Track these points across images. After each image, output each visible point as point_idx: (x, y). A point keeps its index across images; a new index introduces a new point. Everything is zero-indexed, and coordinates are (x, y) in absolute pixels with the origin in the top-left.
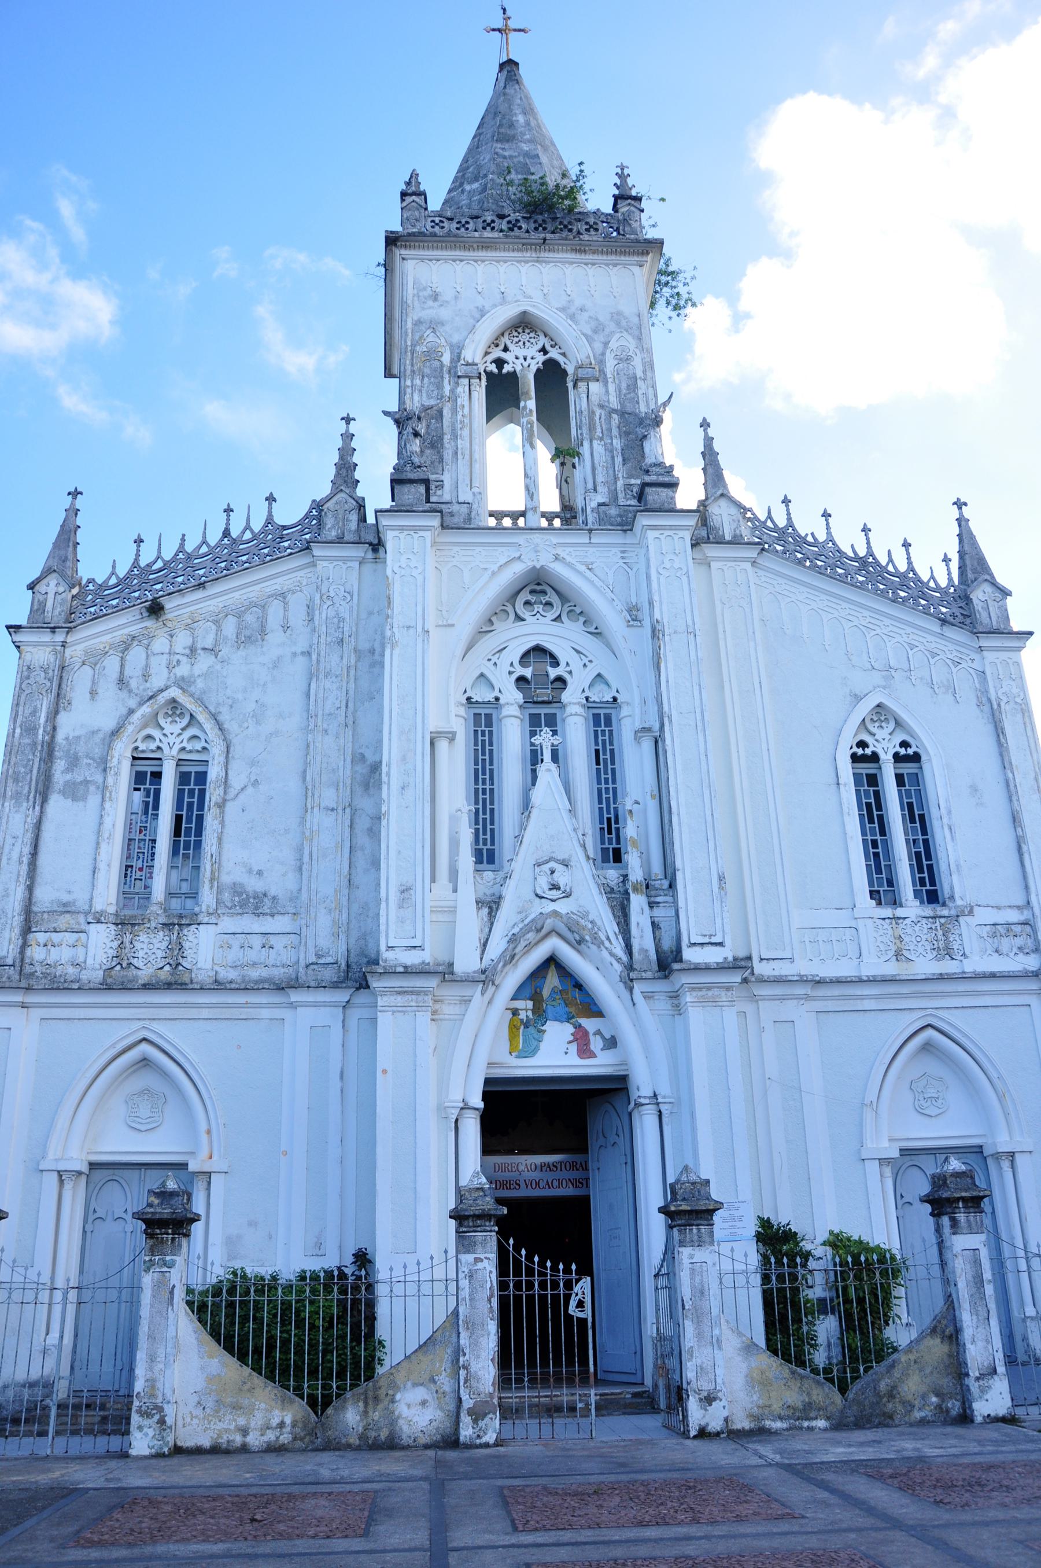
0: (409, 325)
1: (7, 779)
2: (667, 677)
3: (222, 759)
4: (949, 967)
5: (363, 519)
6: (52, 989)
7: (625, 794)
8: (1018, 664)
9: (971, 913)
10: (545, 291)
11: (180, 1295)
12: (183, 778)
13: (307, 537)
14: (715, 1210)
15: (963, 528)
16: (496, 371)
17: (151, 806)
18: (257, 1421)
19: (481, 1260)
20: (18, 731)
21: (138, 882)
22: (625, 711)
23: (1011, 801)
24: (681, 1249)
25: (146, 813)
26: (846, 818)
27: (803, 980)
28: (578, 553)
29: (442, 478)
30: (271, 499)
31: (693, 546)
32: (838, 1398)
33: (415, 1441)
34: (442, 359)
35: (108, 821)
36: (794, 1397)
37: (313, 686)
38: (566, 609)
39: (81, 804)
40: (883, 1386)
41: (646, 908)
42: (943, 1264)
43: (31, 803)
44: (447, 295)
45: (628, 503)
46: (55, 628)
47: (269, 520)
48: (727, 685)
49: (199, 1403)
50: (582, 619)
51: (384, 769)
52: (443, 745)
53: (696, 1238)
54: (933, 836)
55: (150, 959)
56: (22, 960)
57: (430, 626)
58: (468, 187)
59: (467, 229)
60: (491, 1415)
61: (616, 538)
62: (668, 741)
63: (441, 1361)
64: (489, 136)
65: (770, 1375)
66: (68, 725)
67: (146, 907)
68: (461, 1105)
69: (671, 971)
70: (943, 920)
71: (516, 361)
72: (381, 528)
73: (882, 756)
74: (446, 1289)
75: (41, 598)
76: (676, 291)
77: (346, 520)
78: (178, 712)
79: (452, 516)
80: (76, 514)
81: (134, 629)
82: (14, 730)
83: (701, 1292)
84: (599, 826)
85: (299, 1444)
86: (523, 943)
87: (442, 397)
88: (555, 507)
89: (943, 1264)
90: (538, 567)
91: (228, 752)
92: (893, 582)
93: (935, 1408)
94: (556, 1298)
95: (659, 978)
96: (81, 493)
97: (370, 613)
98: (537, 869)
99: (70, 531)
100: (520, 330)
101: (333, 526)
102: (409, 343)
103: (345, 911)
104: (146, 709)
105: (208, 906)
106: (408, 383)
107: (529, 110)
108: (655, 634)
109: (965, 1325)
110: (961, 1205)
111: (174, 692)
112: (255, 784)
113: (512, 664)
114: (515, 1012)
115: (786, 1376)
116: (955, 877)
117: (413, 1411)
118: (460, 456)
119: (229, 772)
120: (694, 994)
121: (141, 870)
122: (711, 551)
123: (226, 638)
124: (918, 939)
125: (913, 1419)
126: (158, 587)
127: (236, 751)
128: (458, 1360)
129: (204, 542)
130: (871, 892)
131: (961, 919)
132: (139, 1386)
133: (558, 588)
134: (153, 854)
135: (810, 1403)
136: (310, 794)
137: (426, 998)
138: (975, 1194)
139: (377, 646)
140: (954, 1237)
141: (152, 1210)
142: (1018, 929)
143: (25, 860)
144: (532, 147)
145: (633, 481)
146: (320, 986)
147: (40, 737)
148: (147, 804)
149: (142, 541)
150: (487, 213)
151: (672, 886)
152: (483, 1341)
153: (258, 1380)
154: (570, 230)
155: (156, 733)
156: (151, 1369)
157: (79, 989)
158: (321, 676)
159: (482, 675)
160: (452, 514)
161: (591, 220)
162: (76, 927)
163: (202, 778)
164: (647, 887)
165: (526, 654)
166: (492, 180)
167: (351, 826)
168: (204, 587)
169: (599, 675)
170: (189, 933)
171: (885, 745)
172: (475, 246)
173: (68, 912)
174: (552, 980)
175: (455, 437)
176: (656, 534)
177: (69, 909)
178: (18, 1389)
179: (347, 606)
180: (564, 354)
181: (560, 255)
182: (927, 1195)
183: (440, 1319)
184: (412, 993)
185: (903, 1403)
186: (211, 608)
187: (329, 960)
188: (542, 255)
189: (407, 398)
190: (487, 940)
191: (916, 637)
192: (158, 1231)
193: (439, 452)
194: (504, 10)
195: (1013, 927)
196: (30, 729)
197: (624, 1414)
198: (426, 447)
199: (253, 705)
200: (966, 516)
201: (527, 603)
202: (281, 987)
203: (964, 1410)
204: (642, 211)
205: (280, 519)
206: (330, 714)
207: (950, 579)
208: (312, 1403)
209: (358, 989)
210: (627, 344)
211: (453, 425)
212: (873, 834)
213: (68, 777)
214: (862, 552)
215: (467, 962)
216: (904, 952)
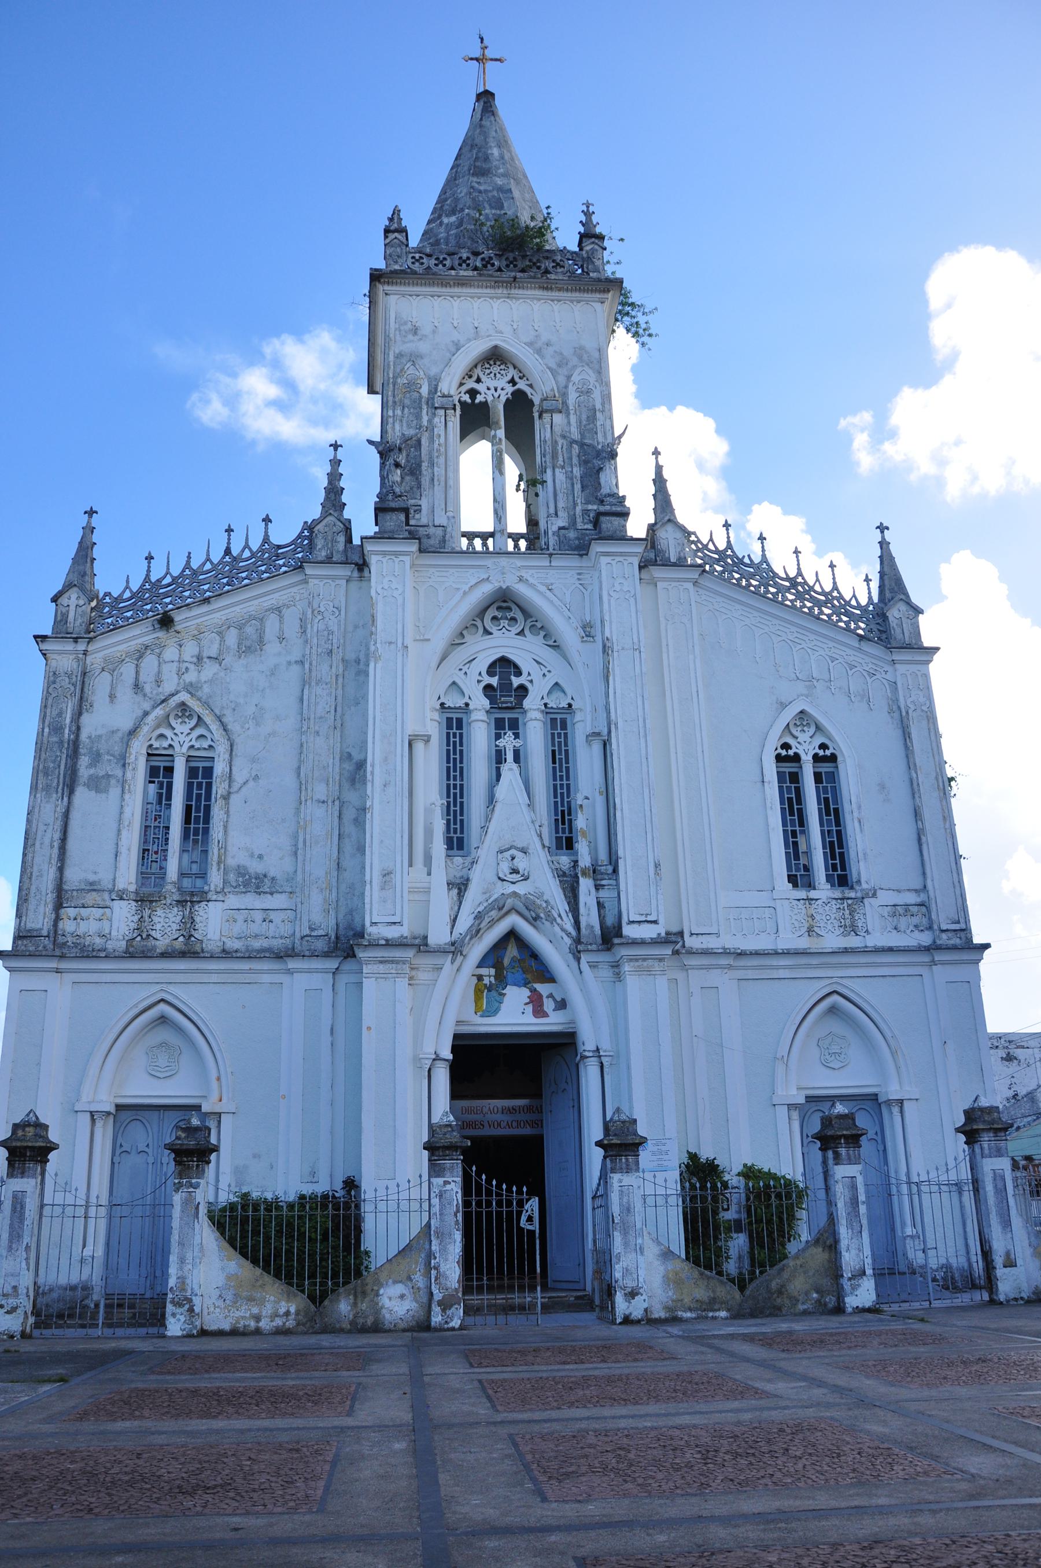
0: (391, 358)
1: (38, 773)
2: (615, 689)
3: (227, 756)
4: (853, 942)
5: (349, 540)
6: (83, 957)
7: (577, 790)
8: (926, 676)
9: (874, 895)
10: (515, 327)
11: (203, 1210)
12: (192, 772)
13: (300, 555)
14: (641, 1144)
15: (884, 550)
16: (469, 401)
17: (165, 796)
18: (268, 1310)
19: (449, 1183)
20: (46, 730)
21: (154, 864)
22: (578, 717)
23: (914, 797)
24: (612, 1175)
25: (160, 803)
26: (769, 812)
27: (726, 952)
28: (539, 575)
29: (420, 503)
30: (267, 520)
31: (641, 568)
32: (737, 1295)
33: (395, 1326)
34: (421, 391)
35: (127, 811)
36: (701, 1293)
37: (306, 692)
38: (529, 624)
39: (104, 795)
40: (774, 1285)
41: (593, 890)
42: (827, 1189)
43: (60, 794)
44: (426, 329)
45: (586, 527)
46: (77, 638)
47: (266, 540)
48: (668, 693)
49: (220, 1296)
50: (542, 633)
51: (369, 769)
52: (419, 746)
53: (624, 1166)
54: (845, 827)
55: (167, 931)
56: (56, 932)
57: (409, 642)
58: (446, 220)
59: (444, 265)
60: (456, 1306)
61: (574, 561)
62: (614, 746)
63: (416, 1263)
64: (466, 168)
65: (683, 1276)
66: (91, 725)
67: (162, 886)
68: (434, 1057)
69: (613, 945)
70: (850, 902)
71: (487, 392)
72: (366, 552)
73: (803, 757)
74: (421, 1206)
75: (64, 610)
76: (635, 320)
77: (334, 541)
78: (187, 714)
79: (429, 538)
80: (92, 532)
81: (147, 639)
82: (43, 729)
83: (628, 1210)
84: (553, 818)
85: (301, 1328)
86: (487, 920)
87: (421, 427)
88: (523, 529)
89: (827, 1189)
90: (504, 587)
91: (232, 750)
92: (819, 600)
93: (816, 1302)
94: (510, 1214)
95: (602, 950)
96: (96, 512)
97: (356, 627)
98: (500, 856)
99: (88, 548)
100: (492, 362)
101: (323, 547)
102: (391, 376)
103: (334, 891)
104: (159, 712)
105: (216, 886)
106: (390, 413)
107: (503, 143)
108: (605, 649)
109: (842, 1237)
110: (842, 1141)
111: (183, 696)
112: (256, 778)
113: (480, 674)
114: (480, 978)
115: (696, 1276)
116: (861, 864)
117: (393, 1302)
118: (436, 483)
119: (233, 768)
120: (632, 964)
121: (156, 853)
122: (657, 572)
123: (228, 648)
124: (828, 917)
125: (797, 1311)
126: (168, 600)
127: (239, 749)
128: (430, 1263)
129: (208, 559)
130: (789, 876)
131: (865, 900)
132: (172, 1282)
133: (522, 604)
134: (167, 839)
135: (714, 1298)
136: (303, 787)
137: (404, 966)
138: (854, 1132)
139: (362, 657)
140: (836, 1167)
141: (179, 1142)
142: (914, 909)
143: (56, 845)
144: (505, 181)
145: (590, 507)
146: (314, 955)
147: (66, 736)
148: (160, 795)
149: (152, 558)
150: (463, 251)
151: (615, 871)
152: (451, 1247)
153: (268, 1279)
154: (539, 268)
155: (168, 733)
156: (181, 1269)
157: (106, 957)
158: (313, 684)
159: (454, 683)
160: (428, 537)
161: (558, 258)
162: (102, 903)
163: (209, 772)
164: (594, 871)
165: (493, 665)
166: (468, 214)
167: (340, 817)
168: (209, 602)
169: (557, 684)
170: (201, 910)
171: (806, 747)
172: (452, 283)
173: (94, 890)
174: (512, 952)
175: (432, 464)
176: (608, 559)
177: (95, 887)
178: (61, 1292)
179: (336, 621)
180: (531, 386)
181: (529, 292)
182: (817, 1133)
183: (416, 1230)
184: (392, 962)
185: (790, 1298)
186: (216, 621)
187: (321, 932)
188: (513, 291)
189: (389, 427)
190: (457, 916)
191: (836, 651)
192: (185, 1159)
193: (417, 479)
194: (482, 39)
195: (910, 907)
196: (57, 729)
197: (567, 1312)
198: (406, 474)
199: (254, 709)
200: (887, 540)
201: (494, 618)
202: (280, 955)
203: (839, 1304)
204: (605, 249)
205: (276, 540)
206: (321, 718)
207: (870, 598)
208: (312, 1298)
209: (345, 958)
210: (588, 377)
211: (430, 453)
212: (793, 824)
213: (92, 771)
214: (792, 573)
215: (439, 935)
216: (815, 929)
